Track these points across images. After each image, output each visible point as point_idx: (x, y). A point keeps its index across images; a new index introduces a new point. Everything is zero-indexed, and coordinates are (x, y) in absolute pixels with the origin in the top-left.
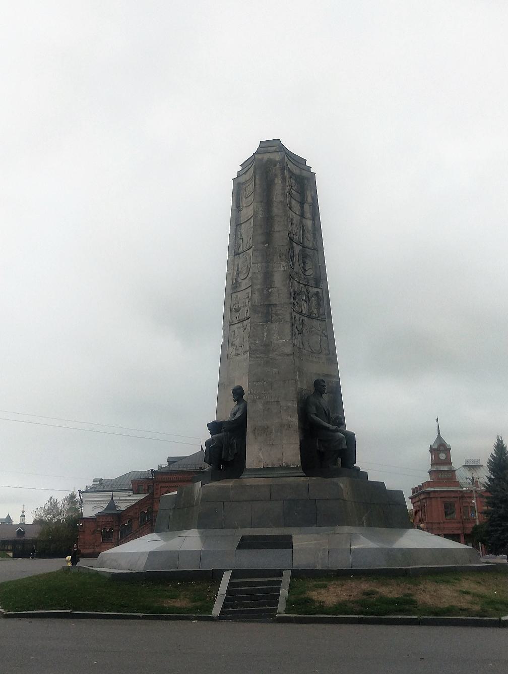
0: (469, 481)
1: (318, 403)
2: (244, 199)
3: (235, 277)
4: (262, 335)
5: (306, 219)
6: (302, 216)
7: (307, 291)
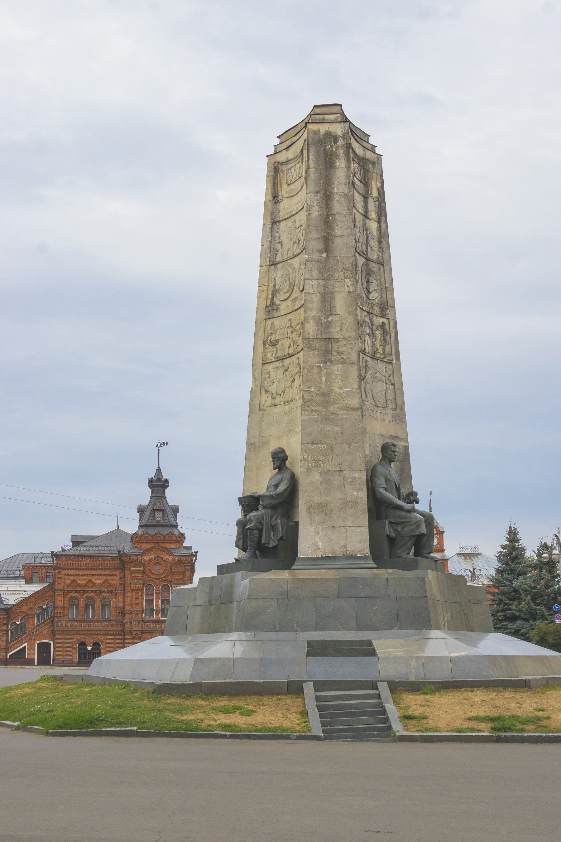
0: (468, 572)
1: (387, 474)
2: (285, 186)
3: (270, 296)
4: (318, 379)
5: (371, 219)
6: (366, 216)
7: (371, 321)
